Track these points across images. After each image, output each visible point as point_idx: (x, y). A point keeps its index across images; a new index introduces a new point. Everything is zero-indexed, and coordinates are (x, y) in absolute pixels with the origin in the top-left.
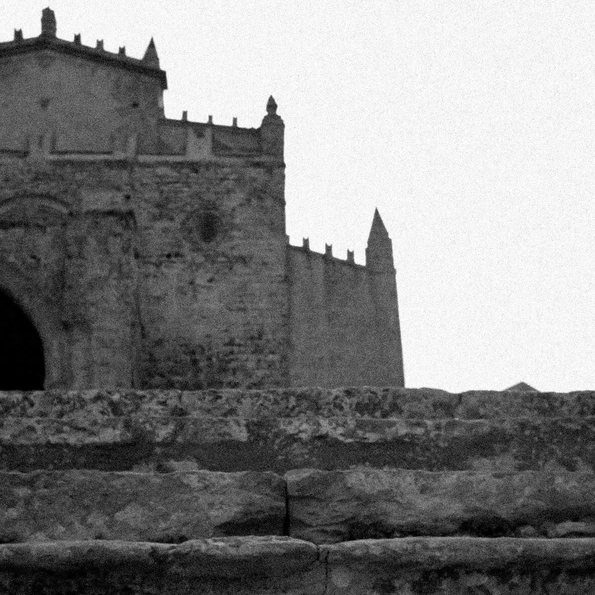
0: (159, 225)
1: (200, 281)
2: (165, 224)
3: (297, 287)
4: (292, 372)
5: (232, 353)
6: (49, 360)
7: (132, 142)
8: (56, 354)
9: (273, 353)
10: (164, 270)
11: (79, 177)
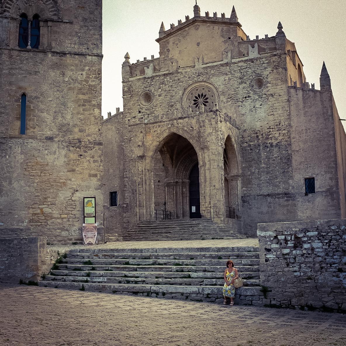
0: (241, 86)
1: (257, 106)
2: (244, 85)
3: (292, 103)
4: (292, 136)
5: (270, 132)
6: (199, 159)
7: (229, 55)
8: (201, 157)
9: (284, 130)
10: (244, 103)
11: (212, 72)
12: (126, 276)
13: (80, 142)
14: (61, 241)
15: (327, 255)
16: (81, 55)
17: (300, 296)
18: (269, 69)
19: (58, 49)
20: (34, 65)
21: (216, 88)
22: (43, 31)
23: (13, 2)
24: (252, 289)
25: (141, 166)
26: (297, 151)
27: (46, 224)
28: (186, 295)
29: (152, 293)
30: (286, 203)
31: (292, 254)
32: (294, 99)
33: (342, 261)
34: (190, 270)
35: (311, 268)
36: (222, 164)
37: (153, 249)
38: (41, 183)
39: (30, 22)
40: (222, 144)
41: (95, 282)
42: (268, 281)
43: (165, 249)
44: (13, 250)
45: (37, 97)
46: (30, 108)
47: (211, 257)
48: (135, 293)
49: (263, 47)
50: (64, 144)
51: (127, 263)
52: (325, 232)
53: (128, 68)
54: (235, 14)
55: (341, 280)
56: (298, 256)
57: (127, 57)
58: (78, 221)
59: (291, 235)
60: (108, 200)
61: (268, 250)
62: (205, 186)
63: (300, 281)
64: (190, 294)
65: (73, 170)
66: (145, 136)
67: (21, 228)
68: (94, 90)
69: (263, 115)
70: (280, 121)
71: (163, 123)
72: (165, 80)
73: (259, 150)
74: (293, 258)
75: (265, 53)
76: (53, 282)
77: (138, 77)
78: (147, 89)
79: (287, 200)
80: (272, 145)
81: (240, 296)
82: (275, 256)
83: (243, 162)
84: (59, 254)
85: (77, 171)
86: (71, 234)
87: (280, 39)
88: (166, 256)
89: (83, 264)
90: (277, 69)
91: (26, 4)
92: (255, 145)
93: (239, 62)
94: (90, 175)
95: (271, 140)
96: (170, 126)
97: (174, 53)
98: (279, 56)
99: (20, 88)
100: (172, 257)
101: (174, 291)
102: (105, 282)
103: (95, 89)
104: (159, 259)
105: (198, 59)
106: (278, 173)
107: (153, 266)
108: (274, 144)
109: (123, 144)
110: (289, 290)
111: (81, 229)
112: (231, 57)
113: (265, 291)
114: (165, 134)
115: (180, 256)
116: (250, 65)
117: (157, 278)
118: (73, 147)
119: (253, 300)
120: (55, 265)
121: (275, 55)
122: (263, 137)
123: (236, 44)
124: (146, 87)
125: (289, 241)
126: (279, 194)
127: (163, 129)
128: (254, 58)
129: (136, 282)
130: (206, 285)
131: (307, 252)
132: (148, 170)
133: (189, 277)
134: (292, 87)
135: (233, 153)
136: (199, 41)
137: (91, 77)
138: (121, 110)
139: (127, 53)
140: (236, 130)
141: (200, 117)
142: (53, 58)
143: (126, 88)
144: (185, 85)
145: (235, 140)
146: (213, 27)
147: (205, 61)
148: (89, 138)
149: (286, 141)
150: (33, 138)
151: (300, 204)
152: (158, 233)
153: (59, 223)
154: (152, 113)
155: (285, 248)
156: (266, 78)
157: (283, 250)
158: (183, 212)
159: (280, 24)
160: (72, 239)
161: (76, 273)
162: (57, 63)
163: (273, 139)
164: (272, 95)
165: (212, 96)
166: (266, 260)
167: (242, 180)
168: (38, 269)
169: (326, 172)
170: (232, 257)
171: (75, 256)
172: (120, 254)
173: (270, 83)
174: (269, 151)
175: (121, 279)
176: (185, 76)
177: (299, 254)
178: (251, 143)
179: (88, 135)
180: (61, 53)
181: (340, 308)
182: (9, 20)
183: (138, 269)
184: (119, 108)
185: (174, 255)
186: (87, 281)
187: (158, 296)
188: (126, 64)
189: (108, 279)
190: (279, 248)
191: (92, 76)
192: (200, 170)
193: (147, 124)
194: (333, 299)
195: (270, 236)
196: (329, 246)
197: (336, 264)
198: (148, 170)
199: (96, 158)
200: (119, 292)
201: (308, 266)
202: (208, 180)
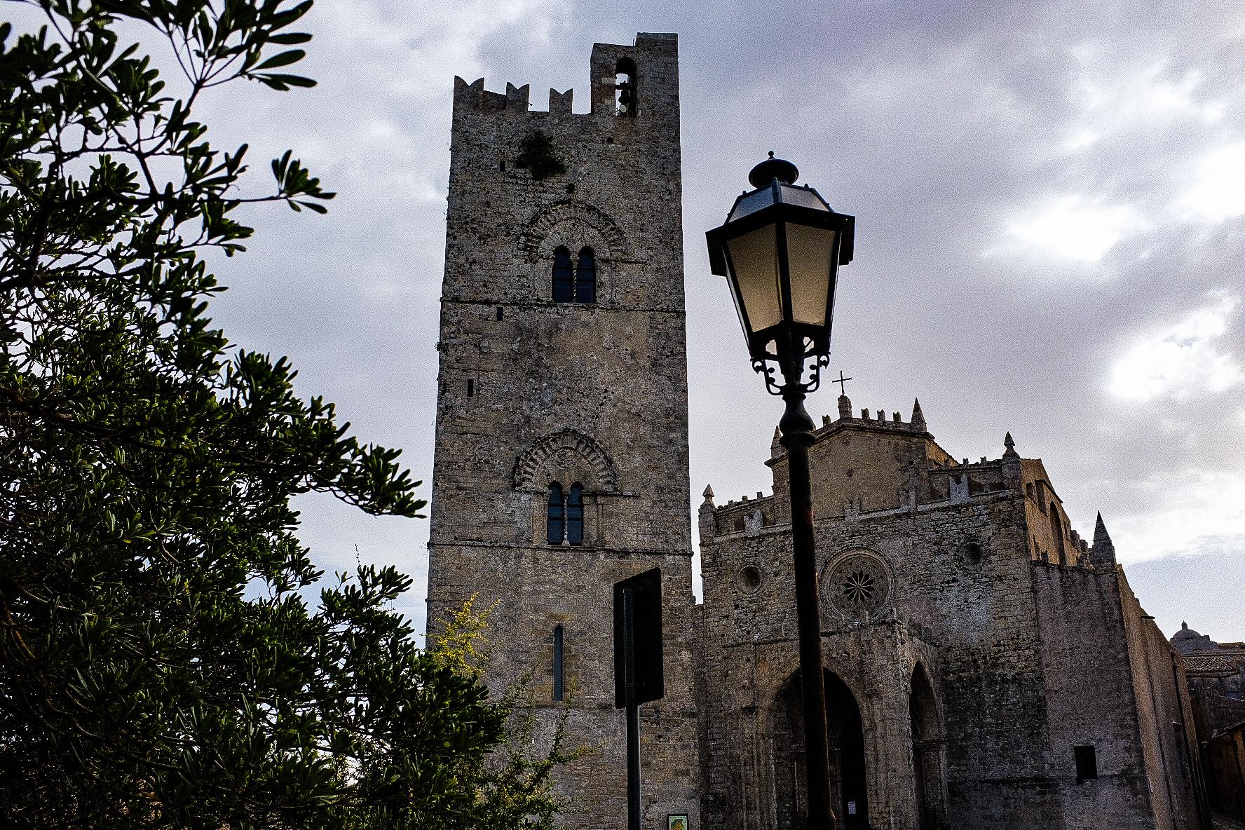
2: (944, 557)
3: (1041, 595)
5: (1000, 651)
7: (913, 497)
8: (865, 712)
9: (1028, 648)
16: (656, 553)
19: (615, 544)
21: (888, 562)
22: (590, 512)
23: (537, 464)
25: (748, 728)
26: (1057, 692)
30: (1039, 799)
32: (1044, 588)
36: (907, 728)
38: (592, 787)
40: (905, 686)
45: (581, 633)
46: (570, 652)
49: (978, 481)
53: (711, 518)
54: (920, 415)
62: (876, 769)
66: (756, 667)
68: (679, 617)
70: (1019, 631)
73: (980, 688)
75: (983, 495)
77: (732, 537)
78: (751, 560)
79: (1042, 793)
83: (949, 712)
87: (1010, 468)
90: (1007, 526)
91: (560, 465)
93: (932, 511)
94: (677, 773)
99: (552, 616)
109: (705, 670)
112: (916, 500)
118: (647, 721)
121: (1002, 499)
122: (986, 663)
123: (925, 475)
126: (1023, 779)
127: (790, 655)
137: (673, 592)
139: (709, 486)
143: (707, 557)
145: (931, 669)
146: (879, 440)
147: (865, 508)
148: (674, 704)
149: (1033, 671)
150: (578, 706)
151: (1068, 801)
154: (761, 609)
156: (987, 544)
159: (1008, 437)
164: (1000, 578)
167: (949, 748)
169: (1116, 736)
174: (1000, 690)
179: (672, 700)
193: (759, 644)
199: (686, 741)
202: (882, 757)
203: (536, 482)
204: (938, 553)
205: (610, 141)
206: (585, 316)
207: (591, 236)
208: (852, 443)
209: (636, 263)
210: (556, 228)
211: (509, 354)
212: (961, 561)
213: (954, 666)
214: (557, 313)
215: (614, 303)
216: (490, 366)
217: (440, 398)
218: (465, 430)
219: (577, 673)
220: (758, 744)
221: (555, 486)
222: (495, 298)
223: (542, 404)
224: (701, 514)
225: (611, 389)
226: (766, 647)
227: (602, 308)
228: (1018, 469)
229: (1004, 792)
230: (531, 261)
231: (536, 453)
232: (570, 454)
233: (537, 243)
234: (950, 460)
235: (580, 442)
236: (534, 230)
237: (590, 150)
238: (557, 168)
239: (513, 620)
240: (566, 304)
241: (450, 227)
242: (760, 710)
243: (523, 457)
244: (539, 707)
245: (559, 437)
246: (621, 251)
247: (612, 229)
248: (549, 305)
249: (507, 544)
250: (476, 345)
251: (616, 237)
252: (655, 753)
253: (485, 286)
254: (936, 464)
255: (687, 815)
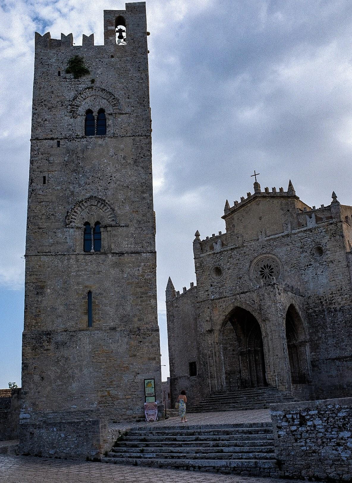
0: (303, 255)
1: (319, 273)
2: (305, 254)
5: (333, 297)
7: (289, 227)
8: (263, 328)
9: (346, 294)
12: (172, 452)
13: (139, 329)
14: (127, 419)
15: (326, 431)
16: (137, 253)
17: (308, 469)
18: (328, 237)
20: (97, 266)
22: (104, 235)
23: (78, 214)
24: (269, 462)
25: (210, 340)
27: (113, 405)
28: (217, 468)
29: (190, 467)
31: (299, 431)
33: (339, 436)
34: (224, 445)
35: (315, 443)
37: (197, 426)
39: (93, 229)
41: (146, 458)
42: (281, 455)
43: (207, 425)
44: (81, 431)
45: (100, 294)
47: (244, 432)
48: (177, 467)
49: (321, 216)
50: (125, 333)
51: (175, 440)
52: (324, 411)
53: (199, 245)
55: (339, 454)
56: (303, 432)
57: (197, 235)
58: (141, 401)
59: (297, 414)
60: (188, 370)
61: (280, 428)
62: (269, 356)
63: (307, 454)
64: (220, 467)
65: (135, 355)
67: (92, 409)
69: (325, 281)
71: (227, 299)
72: (233, 254)
74: (300, 434)
76: (113, 459)
77: (208, 253)
78: (217, 263)
80: (336, 311)
81: (260, 468)
82: (285, 433)
84: (120, 433)
85: (138, 355)
86: (134, 413)
87: (335, 209)
88: (207, 432)
89: (140, 441)
91: (89, 214)
92: (320, 311)
94: (150, 359)
95: (335, 305)
96: (233, 301)
97: (239, 229)
98: (335, 225)
100: (212, 433)
101: (207, 465)
102: (155, 458)
103: (150, 282)
104: (201, 435)
105: (261, 232)
106: (343, 336)
107: (194, 442)
108: (338, 309)
110: (298, 463)
111: (144, 408)
112: (291, 228)
113: (279, 464)
114: (230, 309)
115: (218, 432)
116: (309, 235)
117: (196, 453)
118: (134, 335)
119: (271, 472)
120: (116, 442)
121: (331, 224)
122: (326, 303)
123: (295, 216)
124: (215, 262)
125: (295, 419)
128: (312, 228)
129: (179, 457)
130: (234, 459)
131: (310, 428)
132: (217, 343)
133: (222, 451)
134: (349, 253)
135: (299, 319)
136: (261, 215)
137: (146, 271)
138: (195, 285)
140: (300, 297)
141: (260, 291)
142: (113, 258)
144: (251, 257)
147: (268, 234)
152: (226, 403)
153: (124, 403)
155: (293, 425)
157: (291, 427)
158: (257, 379)
159: (334, 193)
160: (136, 417)
161: (132, 449)
162: (116, 263)
163: (336, 303)
165: (277, 266)
166: (278, 436)
167: (310, 345)
168: (100, 447)
170: (260, 432)
171: (134, 434)
172: (170, 431)
173: (329, 251)
174: (333, 315)
175: (167, 455)
176: (250, 249)
177: (305, 431)
178: (316, 309)
179: (147, 323)
180: (120, 253)
181: (342, 479)
182: (75, 229)
183: (183, 445)
184: (193, 283)
185: (214, 431)
186: (140, 457)
187: (195, 470)
188: (197, 242)
189: (157, 455)
190: (288, 426)
191: (148, 271)
192: (264, 341)
193: (214, 300)
194: (335, 471)
195: (280, 415)
196: (328, 423)
197: (335, 438)
198: (217, 343)
200: (164, 466)
201: (313, 441)
203: (78, 222)
204: (303, 252)
205: (112, 57)
206: (100, 141)
207: (103, 103)
208: (261, 204)
209: (126, 114)
210: (86, 101)
211: (63, 163)
212: (313, 255)
213: (312, 305)
214: (87, 141)
215: (115, 134)
216: (54, 169)
217: (30, 186)
218: (42, 200)
219: (99, 314)
220: (215, 347)
221: (87, 224)
222: (56, 137)
223: (80, 185)
224: (194, 244)
225: (114, 175)
226: (217, 301)
227: (109, 137)
228: (339, 209)
229: (337, 364)
230: (73, 117)
231: (77, 209)
232: (94, 208)
233: (77, 109)
234: (307, 208)
235: (99, 202)
236: (75, 103)
237: (102, 62)
238: (85, 72)
239: (66, 290)
240: (90, 136)
241: (34, 104)
242: (215, 331)
243: (70, 211)
244: (80, 331)
245: (88, 200)
246: (118, 109)
247: (114, 99)
248: (83, 137)
249: (63, 253)
250: (47, 159)
251: (115, 102)
252: (138, 350)
253: (51, 131)
254: (300, 210)
255: (154, 379)
